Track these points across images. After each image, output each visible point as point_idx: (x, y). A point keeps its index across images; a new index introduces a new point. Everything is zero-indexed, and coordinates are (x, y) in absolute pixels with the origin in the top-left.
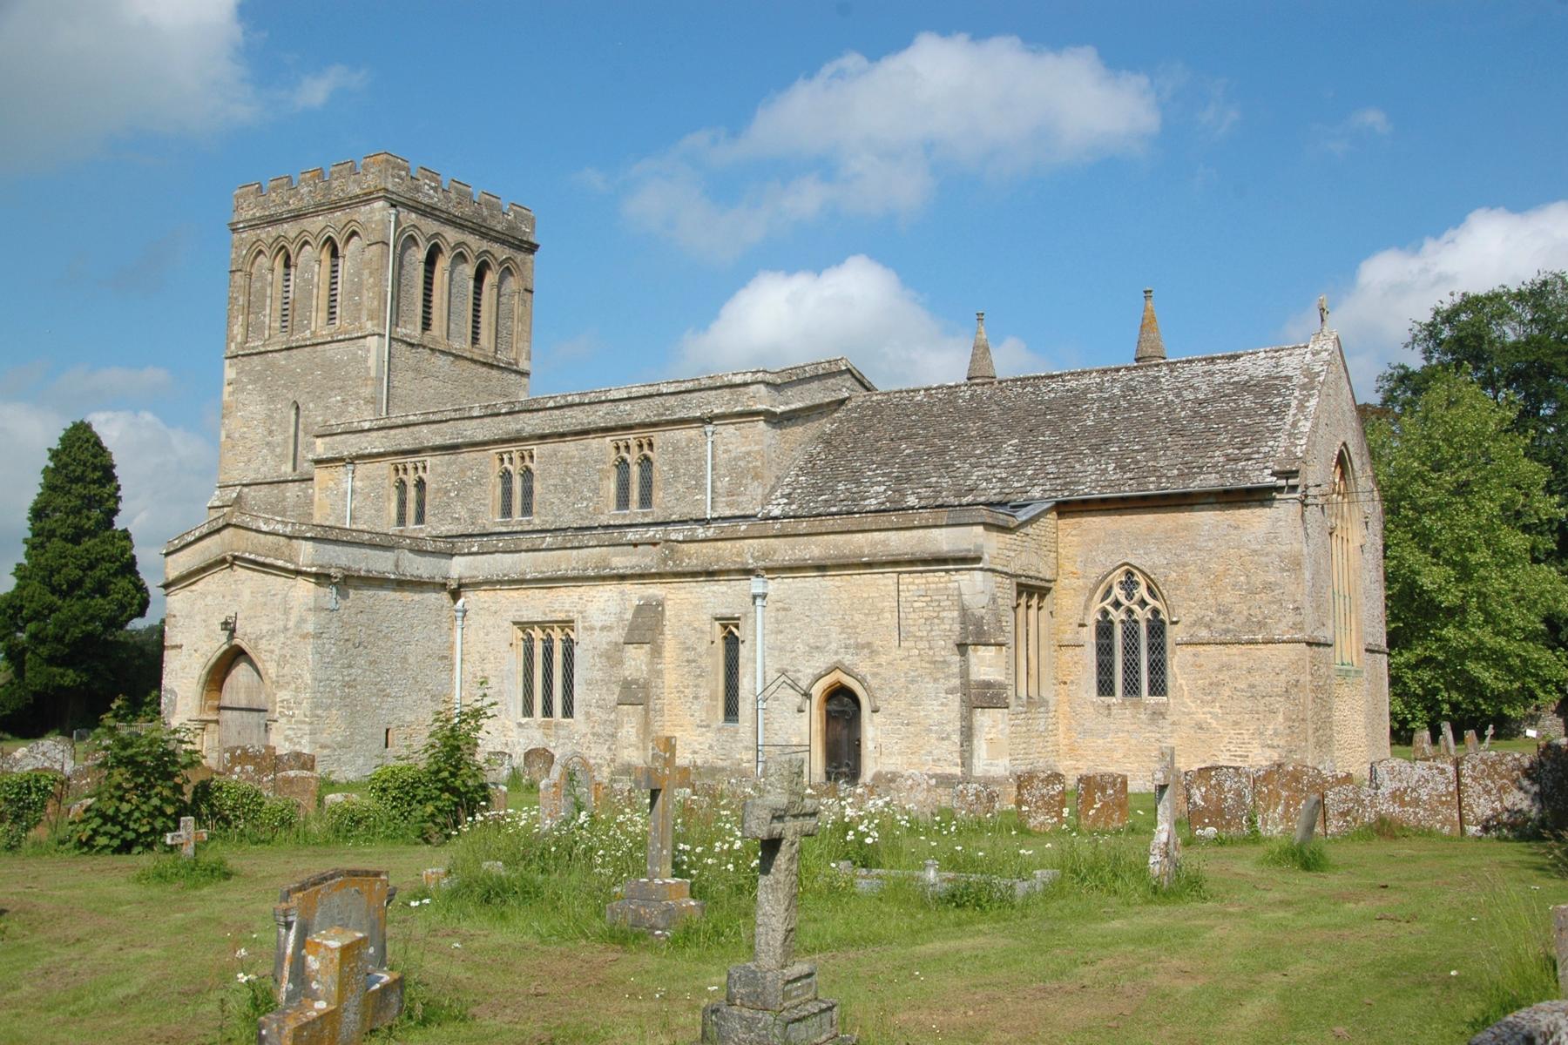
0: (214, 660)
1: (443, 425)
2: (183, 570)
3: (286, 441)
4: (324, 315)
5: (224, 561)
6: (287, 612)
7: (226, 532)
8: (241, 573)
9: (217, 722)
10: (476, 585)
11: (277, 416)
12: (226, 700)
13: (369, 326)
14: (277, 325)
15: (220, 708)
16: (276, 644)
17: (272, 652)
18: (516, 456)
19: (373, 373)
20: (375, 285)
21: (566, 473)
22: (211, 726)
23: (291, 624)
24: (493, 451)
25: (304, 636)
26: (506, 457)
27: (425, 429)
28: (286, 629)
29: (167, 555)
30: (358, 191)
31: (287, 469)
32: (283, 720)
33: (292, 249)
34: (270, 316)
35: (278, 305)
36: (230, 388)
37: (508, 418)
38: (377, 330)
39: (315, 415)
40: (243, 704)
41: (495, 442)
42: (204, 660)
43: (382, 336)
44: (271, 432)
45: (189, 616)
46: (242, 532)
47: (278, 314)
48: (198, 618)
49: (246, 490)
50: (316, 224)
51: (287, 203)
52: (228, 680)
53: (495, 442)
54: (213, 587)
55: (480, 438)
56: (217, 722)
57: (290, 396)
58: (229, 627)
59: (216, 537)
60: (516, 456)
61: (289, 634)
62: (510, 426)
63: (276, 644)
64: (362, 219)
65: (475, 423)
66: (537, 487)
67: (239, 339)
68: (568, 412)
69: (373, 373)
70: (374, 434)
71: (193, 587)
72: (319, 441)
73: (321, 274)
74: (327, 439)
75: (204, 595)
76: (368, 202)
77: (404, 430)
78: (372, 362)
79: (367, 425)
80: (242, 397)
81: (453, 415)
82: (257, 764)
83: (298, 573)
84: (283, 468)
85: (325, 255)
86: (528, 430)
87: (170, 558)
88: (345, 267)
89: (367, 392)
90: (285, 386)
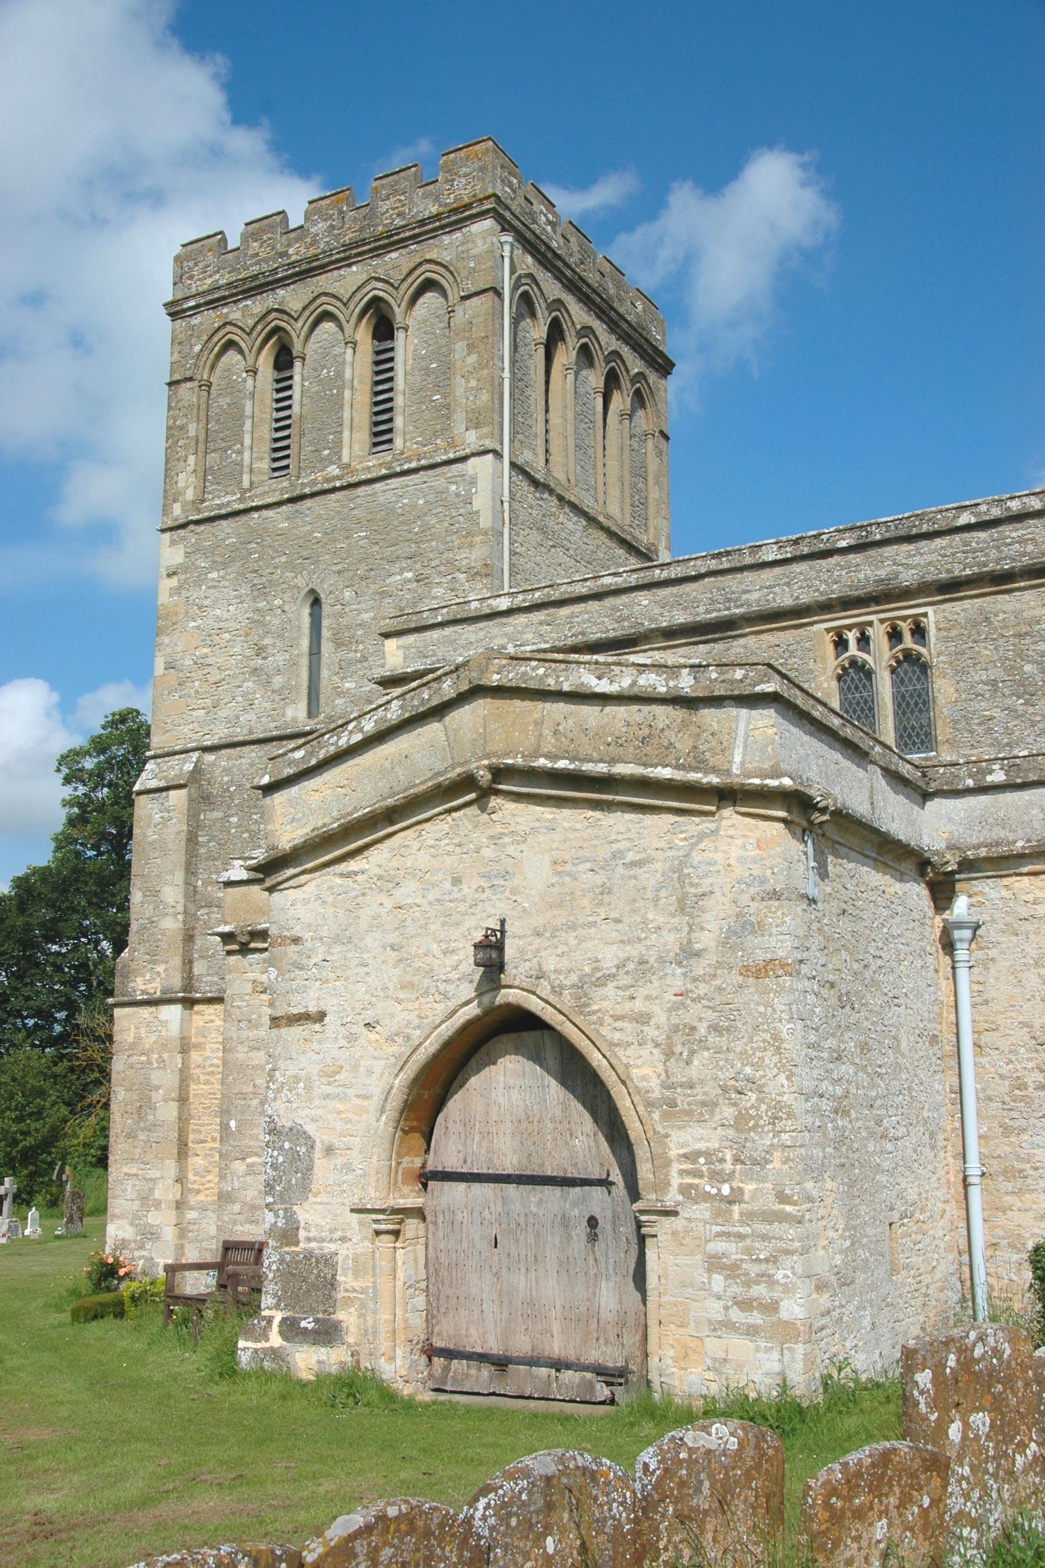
0: (431, 1047)
1: (688, 588)
2: (328, 820)
3: (294, 664)
4: (364, 436)
5: (467, 783)
6: (688, 906)
7: (465, 716)
8: (510, 814)
9: (419, 1213)
10: (1003, 863)
11: (274, 621)
12: (450, 1150)
13: (472, 439)
14: (265, 465)
15: (426, 1178)
16: (657, 998)
17: (642, 1019)
18: (878, 633)
19: (485, 521)
20: (481, 366)
21: (1021, 655)
22: (412, 1226)
23: (706, 940)
24: (820, 629)
25: (761, 971)
26: (851, 636)
27: (643, 598)
28: (689, 953)
29: (269, 789)
30: (434, 210)
31: (296, 714)
32: (701, 1211)
33: (296, 331)
34: (253, 451)
35: (266, 432)
36: (174, 582)
37: (853, 558)
38: (489, 444)
39: (355, 608)
40: (509, 1163)
41: (825, 607)
42: (399, 1048)
43: (498, 454)
44: (260, 651)
45: (343, 938)
46: (518, 705)
47: (267, 446)
48: (372, 941)
49: (210, 758)
50: (347, 281)
51: (284, 254)
52: (454, 1105)
53: (825, 607)
54: (423, 859)
55: (785, 600)
56: (419, 1213)
57: (300, 581)
58: (491, 956)
59: (433, 730)
60: (878, 633)
61: (699, 968)
62: (865, 572)
63: (657, 998)
64: (446, 257)
65: (767, 576)
66: (944, 689)
67: (190, 495)
68: (1011, 532)
69: (485, 521)
70: (522, 619)
71: (353, 865)
72: (391, 644)
73: (358, 364)
74: (411, 639)
75: (389, 882)
76: (457, 225)
77: (593, 605)
78: (482, 502)
79: (504, 604)
80: (196, 594)
81: (713, 564)
82: (997, 1407)
83: (728, 795)
84: (290, 712)
85: (364, 335)
86: (908, 578)
87: (279, 798)
88: (405, 349)
89: (474, 556)
90: (289, 566)
